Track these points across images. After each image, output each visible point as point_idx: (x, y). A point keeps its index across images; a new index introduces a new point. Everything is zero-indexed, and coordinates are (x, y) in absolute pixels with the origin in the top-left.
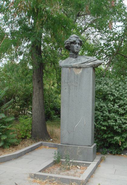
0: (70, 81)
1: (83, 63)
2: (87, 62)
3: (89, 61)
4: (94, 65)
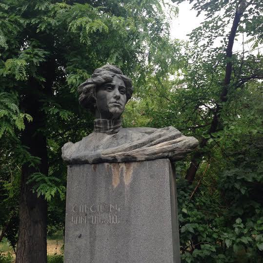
0: (93, 209)
1: (136, 147)
2: (150, 142)
3: (158, 140)
4: (173, 151)
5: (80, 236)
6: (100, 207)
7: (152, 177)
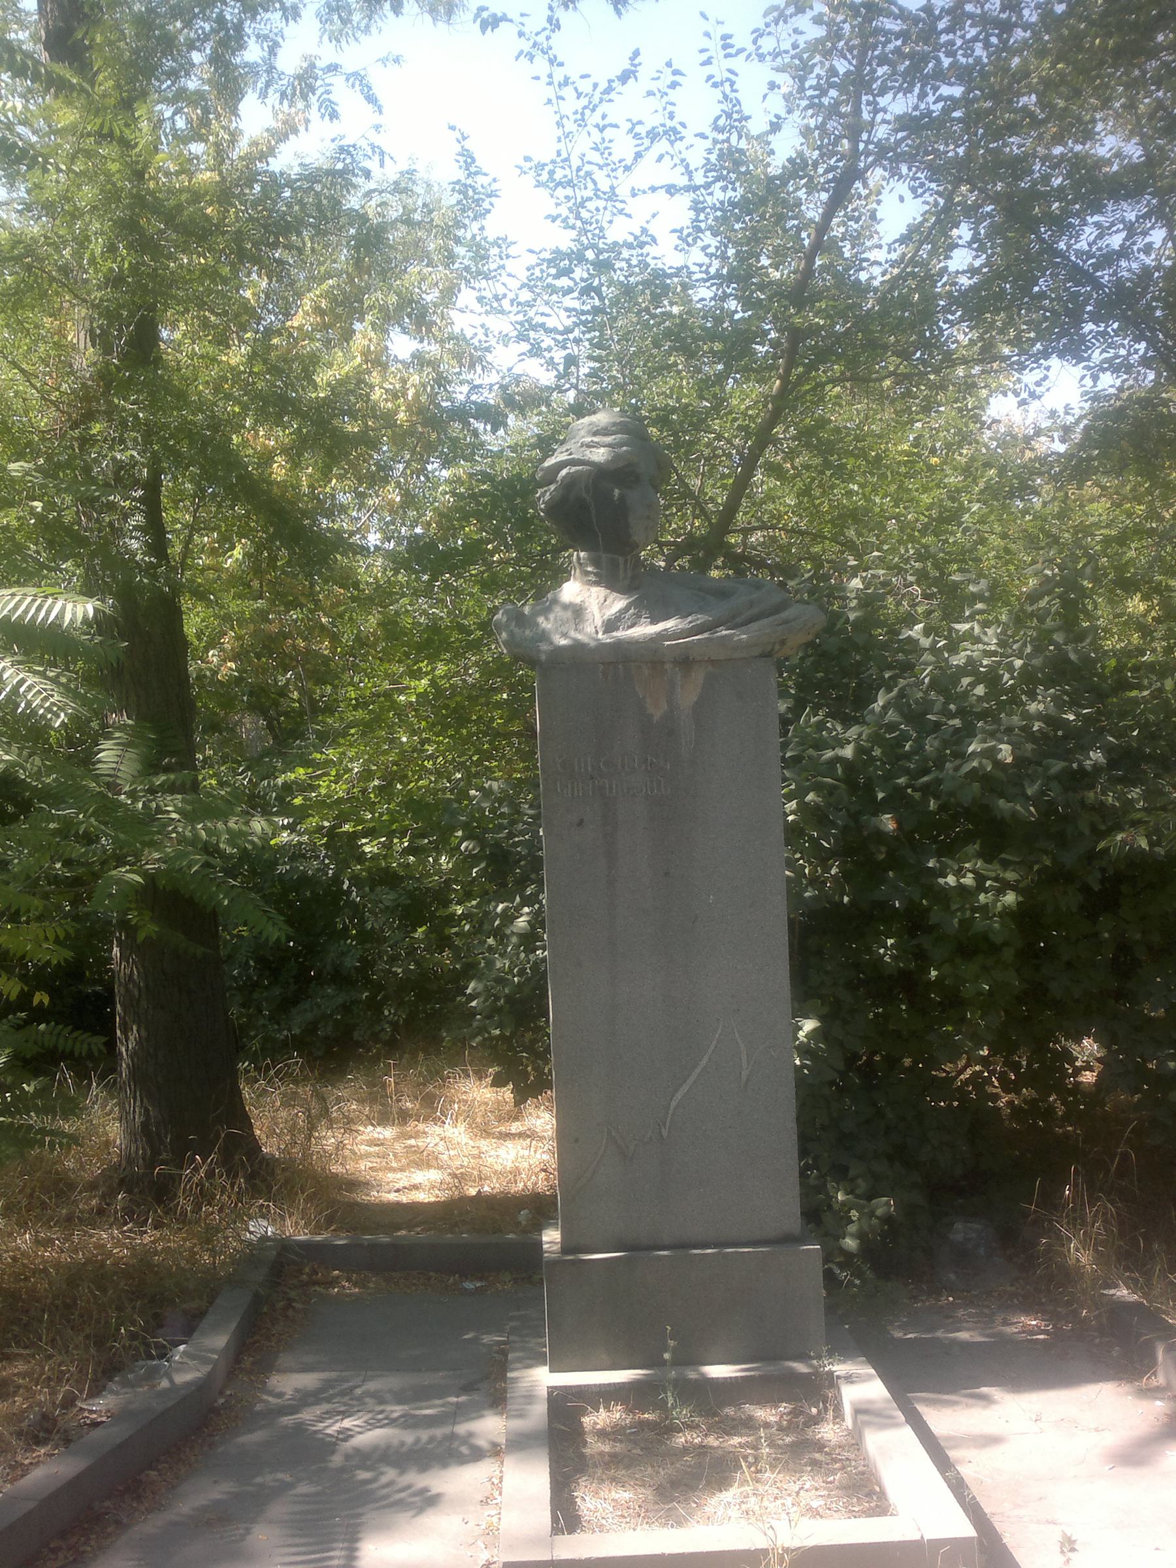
5: (581, 823)
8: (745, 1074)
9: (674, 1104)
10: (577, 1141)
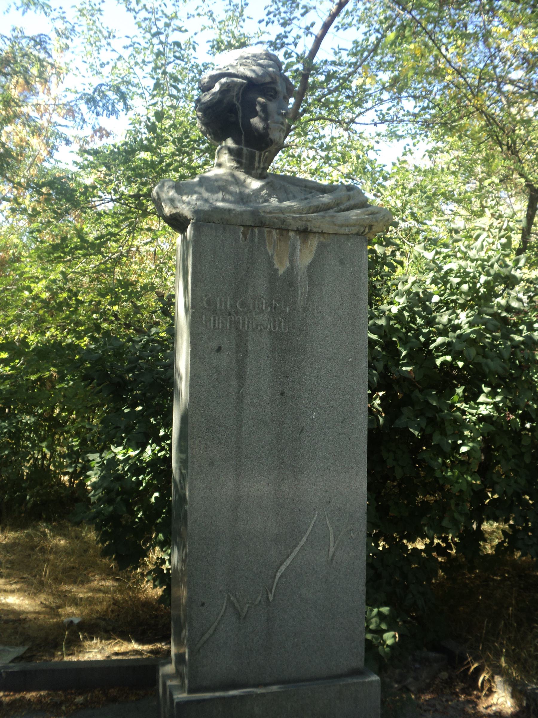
0: (242, 304)
5: (219, 349)
6: (254, 303)
7: (341, 262)
8: (332, 550)
9: (279, 574)
10: (203, 605)
